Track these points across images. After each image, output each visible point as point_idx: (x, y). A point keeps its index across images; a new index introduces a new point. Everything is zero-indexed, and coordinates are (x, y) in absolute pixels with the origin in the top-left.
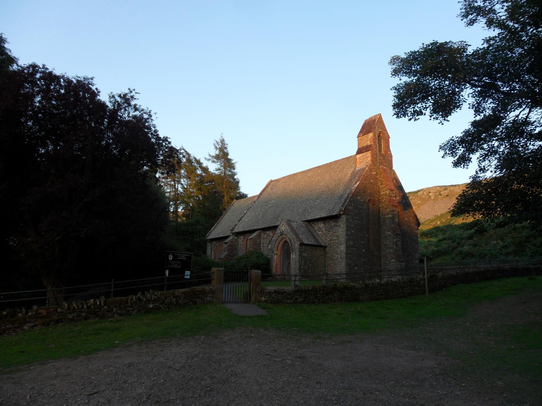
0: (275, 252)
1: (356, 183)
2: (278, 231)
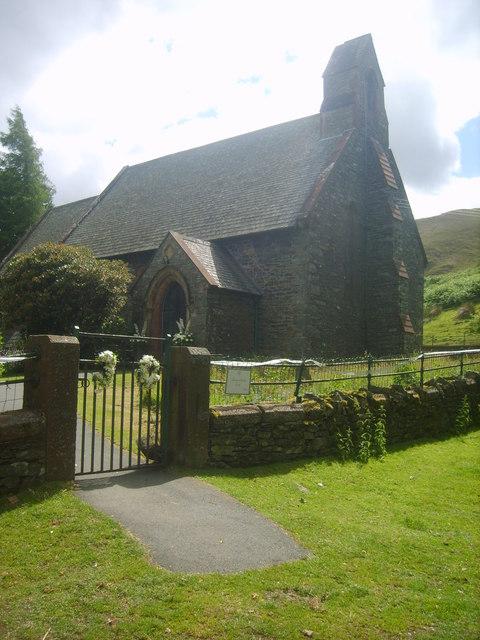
0: (149, 306)
1: (328, 164)
2: (157, 261)
